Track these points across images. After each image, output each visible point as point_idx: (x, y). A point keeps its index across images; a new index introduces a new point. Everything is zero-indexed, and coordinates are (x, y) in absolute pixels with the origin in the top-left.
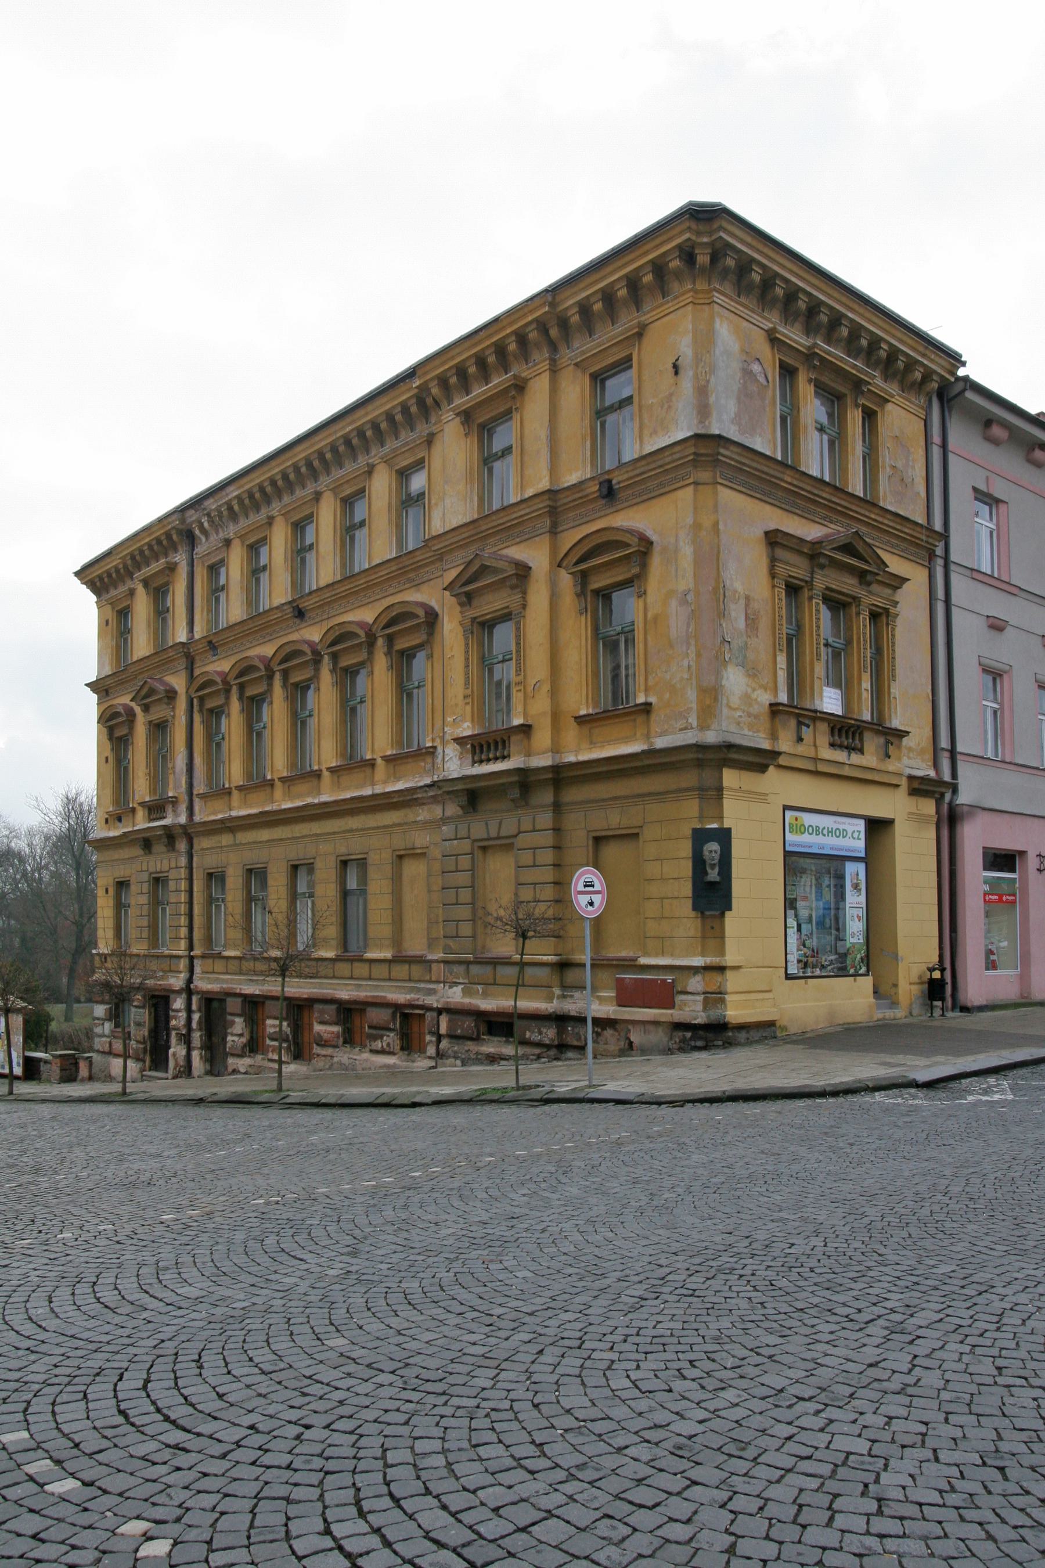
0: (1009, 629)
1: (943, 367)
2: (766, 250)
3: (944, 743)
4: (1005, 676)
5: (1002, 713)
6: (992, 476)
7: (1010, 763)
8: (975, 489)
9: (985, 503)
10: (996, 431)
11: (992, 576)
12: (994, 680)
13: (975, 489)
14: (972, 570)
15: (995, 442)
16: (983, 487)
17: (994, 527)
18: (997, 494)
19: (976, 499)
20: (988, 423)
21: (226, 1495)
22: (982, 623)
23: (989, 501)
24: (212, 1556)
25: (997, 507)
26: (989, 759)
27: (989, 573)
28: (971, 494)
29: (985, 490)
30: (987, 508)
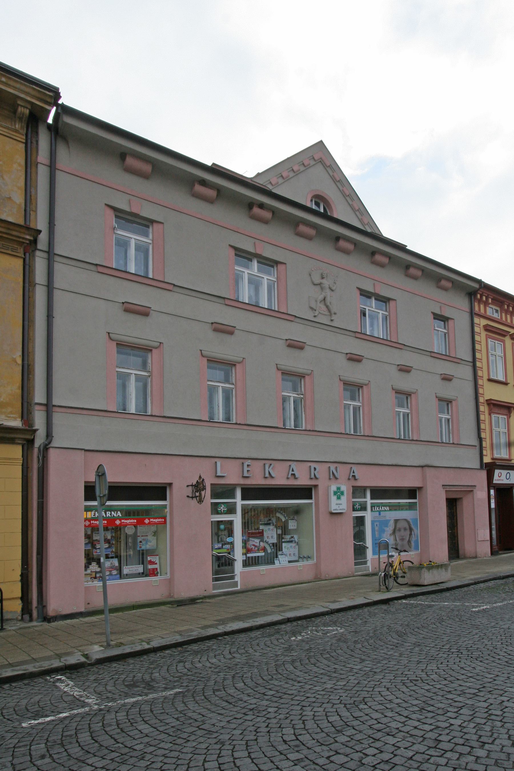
0: (454, 379)
1: (33, 97)
2: (18, 86)
3: (39, 396)
4: (454, 402)
5: (452, 421)
6: (257, 242)
7: (417, 440)
8: (434, 314)
9: (442, 321)
10: (444, 283)
11: (361, 333)
12: (448, 404)
13: (434, 314)
14: (431, 352)
15: (415, 278)
16: (438, 312)
17: (275, 280)
18: (447, 315)
19: (435, 318)
20: (123, 156)
21: (135, 766)
22: (438, 378)
23: (443, 319)
24: (219, 759)
25: (277, 266)
26: (352, 435)
27: (444, 354)
28: (432, 316)
29: (440, 313)
30: (443, 323)
